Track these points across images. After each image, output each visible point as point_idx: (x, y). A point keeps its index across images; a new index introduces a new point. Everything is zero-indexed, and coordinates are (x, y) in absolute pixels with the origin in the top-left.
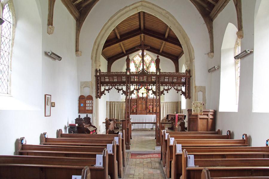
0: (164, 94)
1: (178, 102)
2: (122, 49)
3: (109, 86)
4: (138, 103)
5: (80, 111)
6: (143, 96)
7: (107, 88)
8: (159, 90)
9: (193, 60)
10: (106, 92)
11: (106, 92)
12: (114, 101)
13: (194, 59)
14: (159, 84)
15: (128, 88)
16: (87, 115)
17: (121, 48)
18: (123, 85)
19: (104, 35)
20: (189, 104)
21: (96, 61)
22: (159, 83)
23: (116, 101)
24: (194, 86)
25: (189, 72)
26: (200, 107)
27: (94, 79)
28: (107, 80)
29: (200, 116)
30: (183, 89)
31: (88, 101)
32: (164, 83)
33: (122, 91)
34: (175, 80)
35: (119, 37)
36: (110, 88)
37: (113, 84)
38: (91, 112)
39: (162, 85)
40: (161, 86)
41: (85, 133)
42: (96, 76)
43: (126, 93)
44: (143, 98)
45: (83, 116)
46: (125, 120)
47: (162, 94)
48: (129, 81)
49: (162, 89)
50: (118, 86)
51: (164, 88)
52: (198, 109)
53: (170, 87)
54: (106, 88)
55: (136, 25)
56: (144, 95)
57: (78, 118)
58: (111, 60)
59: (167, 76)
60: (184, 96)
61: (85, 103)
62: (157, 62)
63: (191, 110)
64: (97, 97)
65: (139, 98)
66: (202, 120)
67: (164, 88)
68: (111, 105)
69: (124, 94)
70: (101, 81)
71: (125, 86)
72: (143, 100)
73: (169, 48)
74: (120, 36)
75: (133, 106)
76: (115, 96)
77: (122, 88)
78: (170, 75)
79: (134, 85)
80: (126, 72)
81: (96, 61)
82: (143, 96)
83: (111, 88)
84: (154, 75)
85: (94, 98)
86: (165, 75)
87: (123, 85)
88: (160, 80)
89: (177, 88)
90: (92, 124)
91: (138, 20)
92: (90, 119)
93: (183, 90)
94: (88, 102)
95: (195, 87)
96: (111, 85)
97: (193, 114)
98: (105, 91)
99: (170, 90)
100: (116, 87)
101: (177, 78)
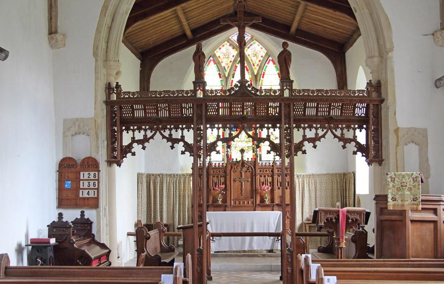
0: (304, 152)
1: (344, 174)
2: (182, 26)
3: (145, 130)
4: (228, 177)
5: (63, 201)
6: (242, 157)
8: (290, 140)
10: (137, 148)
12: (159, 173)
13: (392, 50)
14: (289, 124)
15: (200, 136)
16: (82, 213)
17: (180, 22)
20: (378, 180)
23: (164, 172)
24: (391, 128)
25: (376, 87)
26: (410, 190)
27: (103, 111)
28: (139, 114)
29: (411, 215)
30: (361, 136)
31: (86, 173)
32: (305, 121)
34: (335, 113)
35: (189, 33)
37: (156, 124)
38: (94, 203)
41: (78, 264)
42: (109, 103)
43: (195, 149)
44: (243, 163)
45: (71, 215)
46: (192, 227)
47: (300, 153)
49: (297, 136)
50: (170, 129)
51: (304, 136)
52: (407, 193)
53: (321, 133)
56: (245, 154)
57: (56, 220)
58: (149, 56)
59: (312, 101)
60: (364, 158)
61: (78, 180)
62: (284, 61)
63: (386, 196)
64: (110, 163)
65: (231, 165)
66: (418, 225)
67: (304, 136)
68: (150, 186)
70: (121, 117)
71: (191, 131)
72: (244, 169)
73: (320, 21)
75: (215, 187)
76: (164, 158)
77: (183, 137)
78: (320, 98)
80: (194, 91)
82: (242, 157)
83: (152, 137)
84: (274, 99)
85: (103, 166)
86: (306, 98)
87: (186, 128)
88: (291, 112)
89: (342, 134)
90: (96, 239)
92: (92, 223)
93: (359, 140)
94: (84, 175)
95: (397, 131)
96: (151, 129)
97: (390, 208)
98: (135, 145)
99: (322, 139)
101: (342, 106)
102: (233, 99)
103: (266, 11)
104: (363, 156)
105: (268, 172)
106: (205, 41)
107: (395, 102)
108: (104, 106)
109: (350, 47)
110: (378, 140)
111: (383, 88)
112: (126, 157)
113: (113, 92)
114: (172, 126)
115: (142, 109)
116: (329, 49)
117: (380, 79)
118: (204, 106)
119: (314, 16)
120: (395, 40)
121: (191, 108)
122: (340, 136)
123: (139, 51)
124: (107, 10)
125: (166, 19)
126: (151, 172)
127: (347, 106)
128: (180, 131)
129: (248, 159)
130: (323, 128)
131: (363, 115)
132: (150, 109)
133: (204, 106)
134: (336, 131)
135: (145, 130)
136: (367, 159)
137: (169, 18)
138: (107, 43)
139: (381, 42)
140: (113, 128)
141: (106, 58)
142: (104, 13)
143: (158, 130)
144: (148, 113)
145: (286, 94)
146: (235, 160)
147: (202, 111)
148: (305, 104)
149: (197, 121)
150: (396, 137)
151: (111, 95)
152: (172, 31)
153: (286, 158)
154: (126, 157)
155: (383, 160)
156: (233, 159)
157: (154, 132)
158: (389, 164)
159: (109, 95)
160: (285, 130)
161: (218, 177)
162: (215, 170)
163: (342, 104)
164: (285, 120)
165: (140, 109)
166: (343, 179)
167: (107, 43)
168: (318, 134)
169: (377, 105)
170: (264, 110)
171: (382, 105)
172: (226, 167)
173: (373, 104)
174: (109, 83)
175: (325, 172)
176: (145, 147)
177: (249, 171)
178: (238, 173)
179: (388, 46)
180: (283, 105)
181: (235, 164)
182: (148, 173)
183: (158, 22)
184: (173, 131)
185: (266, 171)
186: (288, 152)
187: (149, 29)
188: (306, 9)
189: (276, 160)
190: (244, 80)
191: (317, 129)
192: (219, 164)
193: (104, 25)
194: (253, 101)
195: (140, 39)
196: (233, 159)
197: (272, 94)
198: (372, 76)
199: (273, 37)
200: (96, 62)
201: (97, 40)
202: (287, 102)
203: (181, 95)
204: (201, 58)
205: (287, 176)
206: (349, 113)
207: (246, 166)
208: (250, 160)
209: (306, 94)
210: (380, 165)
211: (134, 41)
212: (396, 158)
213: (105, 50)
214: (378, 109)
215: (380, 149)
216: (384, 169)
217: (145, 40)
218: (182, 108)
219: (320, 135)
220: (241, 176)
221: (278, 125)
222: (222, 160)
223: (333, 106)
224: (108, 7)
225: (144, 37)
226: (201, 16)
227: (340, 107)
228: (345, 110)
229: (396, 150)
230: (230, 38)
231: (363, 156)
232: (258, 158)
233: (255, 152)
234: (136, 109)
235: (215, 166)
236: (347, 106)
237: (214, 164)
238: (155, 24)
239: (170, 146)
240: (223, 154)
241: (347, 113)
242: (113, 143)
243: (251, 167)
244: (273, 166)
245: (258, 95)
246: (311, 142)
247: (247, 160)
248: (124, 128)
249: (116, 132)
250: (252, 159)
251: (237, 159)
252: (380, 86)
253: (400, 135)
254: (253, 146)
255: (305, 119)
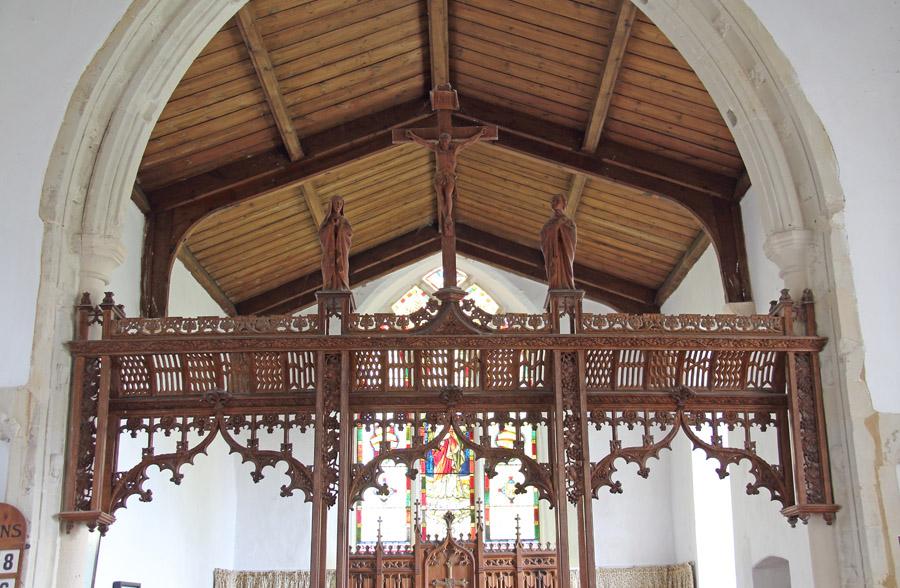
1: (669, 569)
3: (184, 429)
4: (419, 577)
6: (449, 530)
7: (165, 444)
8: (580, 453)
9: (836, 219)
10: (156, 478)
11: (156, 478)
12: (267, 569)
13: (840, 207)
14: (576, 408)
15: (333, 442)
18: (292, 417)
19: (151, 49)
21: (82, 230)
22: (577, 398)
23: (278, 568)
24: (857, 415)
27: (60, 369)
28: (169, 383)
32: (615, 402)
33: (283, 466)
35: (293, 145)
36: (191, 447)
39: (598, 420)
40: (591, 427)
42: (78, 348)
43: (317, 481)
44: (450, 544)
47: (604, 490)
48: (338, 385)
50: (254, 426)
51: (615, 443)
53: (657, 434)
54: (154, 445)
55: (398, 63)
56: (455, 525)
60: (778, 504)
64: (67, 524)
65: (425, 550)
67: (385, 444)
69: (299, 494)
70: (113, 394)
71: (311, 430)
72: (454, 559)
73: (610, 232)
74: (305, 142)
77: (287, 446)
79: (379, 416)
81: (82, 230)
82: (449, 530)
83: (201, 448)
84: (530, 340)
87: (296, 422)
89: (716, 438)
91: (414, 26)
95: (873, 421)
96: (201, 425)
98: (152, 470)
100: (243, 437)
101: (712, 361)
102: (423, 339)
103: (499, 218)
104: (774, 498)
105: (504, 565)
106: (372, 283)
107: (860, 344)
108: (66, 359)
109: (672, 291)
110: (818, 452)
111: (819, 310)
112: (123, 505)
113: (96, 319)
114: (259, 418)
115: (177, 369)
116: (628, 299)
117: (810, 287)
118: (345, 357)
119: (597, 221)
120: (847, 181)
121: (310, 365)
122: (710, 443)
123: (233, 299)
124: (88, 98)
125: (286, 222)
126: (248, 568)
127: (726, 360)
128: (278, 430)
129: (461, 535)
130: (663, 419)
131: (767, 386)
132: (198, 369)
133: (345, 357)
134: (699, 429)
135: (184, 429)
136: (785, 507)
137: (291, 220)
138: (88, 187)
139: (808, 191)
140: (87, 419)
141: (82, 227)
142: (79, 104)
143: (218, 427)
144: (194, 380)
145: (565, 327)
146: (433, 539)
147: (339, 374)
148: (616, 353)
149: (325, 400)
150: (872, 440)
151: (90, 328)
152: (300, 257)
153: (569, 503)
154: (123, 505)
155: (838, 508)
156: (429, 536)
157: (207, 433)
158: (859, 517)
159: (81, 328)
160: (565, 425)
161: (396, 577)
162: (390, 562)
163: (714, 354)
164: (564, 396)
165: (171, 370)
166: (668, 580)
167: (88, 187)
168: (652, 437)
169: (808, 354)
170: (507, 373)
171: (821, 354)
172: (413, 553)
173: (797, 354)
174: (87, 295)
175: (626, 564)
176: (182, 476)
177: (465, 563)
178: (439, 567)
179: (829, 198)
180: (557, 356)
181: (434, 548)
182: (241, 569)
183: (267, 230)
184: (262, 432)
185: (501, 562)
186: (574, 487)
187: (250, 246)
188: (582, 203)
189: (521, 537)
190: (453, 288)
191: (646, 423)
192: (399, 547)
193: (79, 135)
194: (478, 346)
195: (231, 269)
196: (429, 536)
197: (527, 326)
198: (786, 281)
199: (512, 276)
200: (45, 234)
201: (54, 171)
202: (570, 349)
203: (283, 329)
204: (340, 233)
205: (545, 574)
206: (730, 380)
207: (457, 551)
208: (465, 538)
209: (617, 326)
210: (829, 524)
211: (218, 274)
212: (880, 500)
213: (80, 207)
214: (811, 366)
215: (826, 475)
216: (842, 534)
217: (243, 273)
218: (286, 366)
219: (657, 440)
220: (447, 575)
221: (545, 415)
222: (405, 539)
223: (689, 360)
224: (90, 90)
225: (239, 266)
226: (364, 224)
227: (707, 364)
228: (719, 372)
229: (877, 477)
230: (424, 279)
231: (774, 498)
232: (484, 532)
233: (477, 520)
234: (160, 370)
235: (390, 552)
236: (726, 360)
237: (387, 549)
238: (263, 232)
239: (252, 474)
240: (409, 525)
241: (725, 380)
242: (84, 462)
243: (468, 554)
244: (515, 551)
245: (490, 330)
246: (634, 459)
247: (458, 538)
248: (124, 422)
249: (95, 431)
250: (469, 535)
251: (437, 536)
252: (812, 305)
253: (885, 432)
254: (472, 508)
255: (617, 396)
